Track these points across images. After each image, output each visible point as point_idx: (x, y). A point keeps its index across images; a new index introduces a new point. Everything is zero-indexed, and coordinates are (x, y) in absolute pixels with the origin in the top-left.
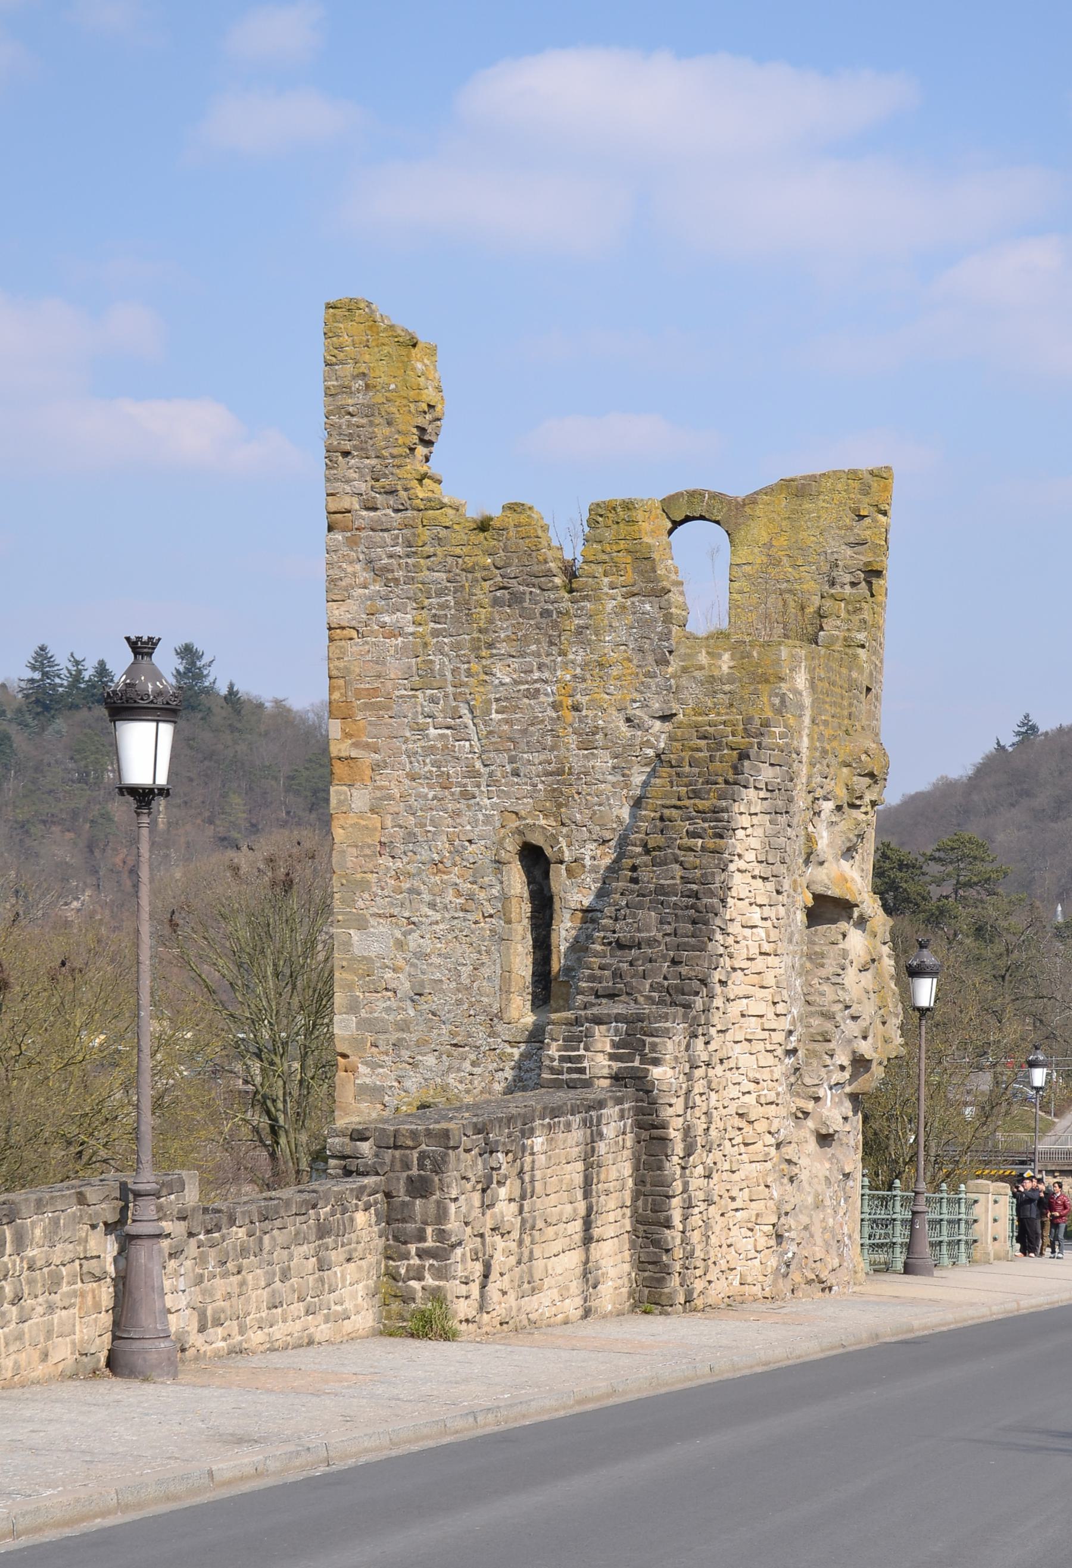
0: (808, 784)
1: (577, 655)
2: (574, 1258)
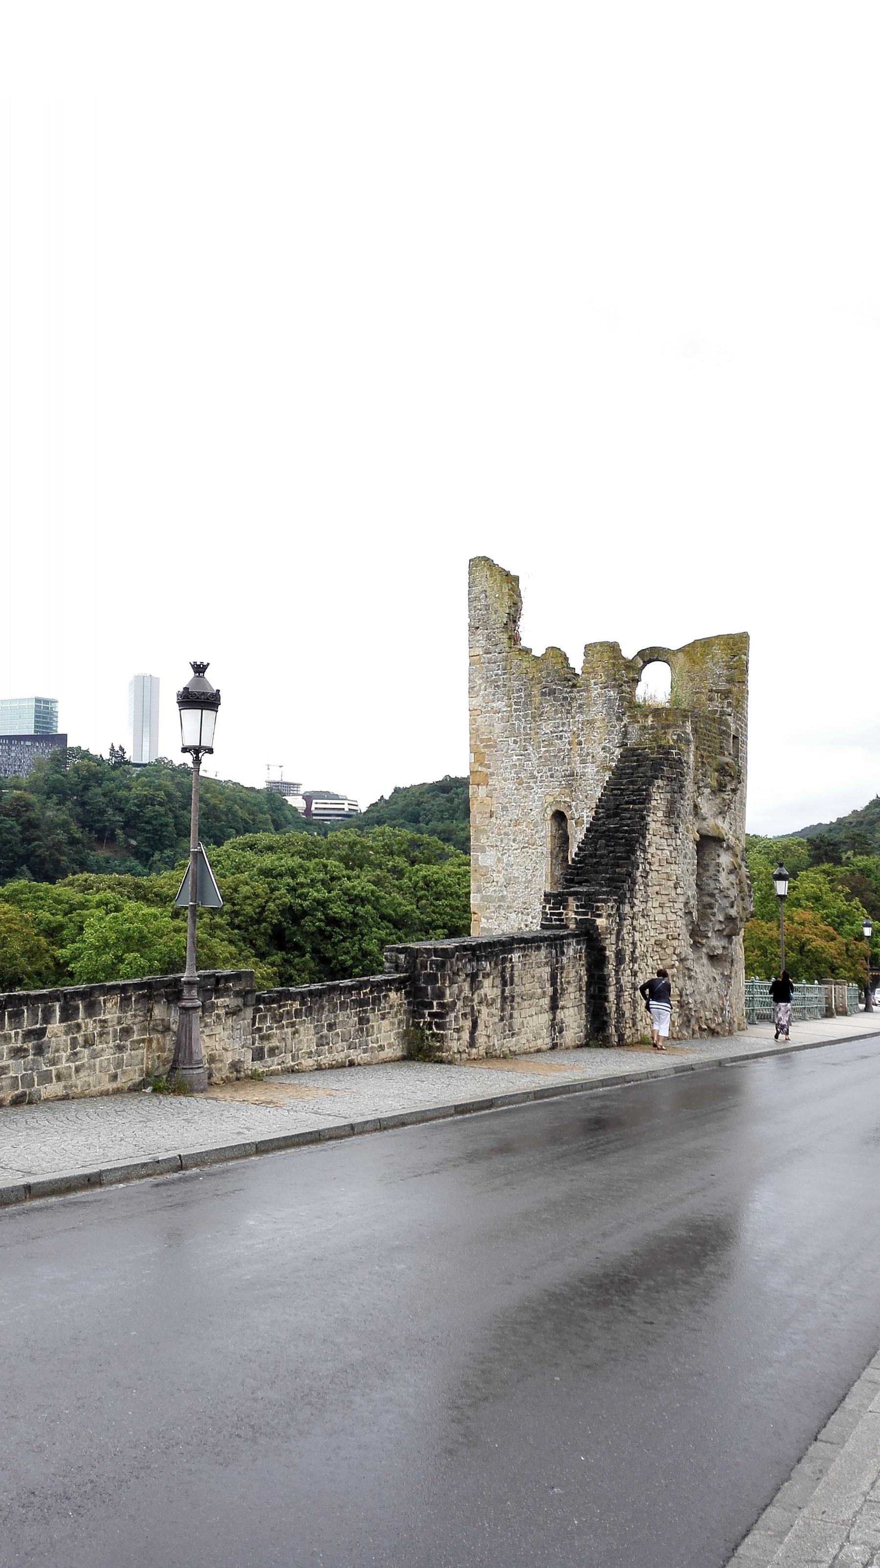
0: (694, 779)
1: (580, 717)
2: (546, 1018)
